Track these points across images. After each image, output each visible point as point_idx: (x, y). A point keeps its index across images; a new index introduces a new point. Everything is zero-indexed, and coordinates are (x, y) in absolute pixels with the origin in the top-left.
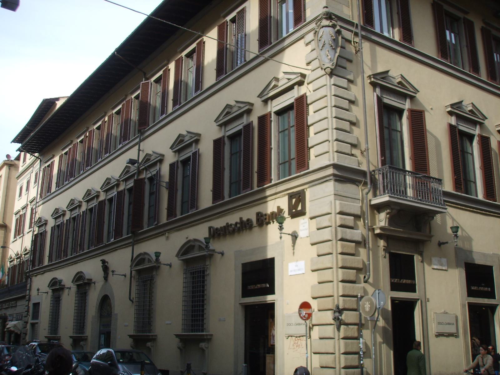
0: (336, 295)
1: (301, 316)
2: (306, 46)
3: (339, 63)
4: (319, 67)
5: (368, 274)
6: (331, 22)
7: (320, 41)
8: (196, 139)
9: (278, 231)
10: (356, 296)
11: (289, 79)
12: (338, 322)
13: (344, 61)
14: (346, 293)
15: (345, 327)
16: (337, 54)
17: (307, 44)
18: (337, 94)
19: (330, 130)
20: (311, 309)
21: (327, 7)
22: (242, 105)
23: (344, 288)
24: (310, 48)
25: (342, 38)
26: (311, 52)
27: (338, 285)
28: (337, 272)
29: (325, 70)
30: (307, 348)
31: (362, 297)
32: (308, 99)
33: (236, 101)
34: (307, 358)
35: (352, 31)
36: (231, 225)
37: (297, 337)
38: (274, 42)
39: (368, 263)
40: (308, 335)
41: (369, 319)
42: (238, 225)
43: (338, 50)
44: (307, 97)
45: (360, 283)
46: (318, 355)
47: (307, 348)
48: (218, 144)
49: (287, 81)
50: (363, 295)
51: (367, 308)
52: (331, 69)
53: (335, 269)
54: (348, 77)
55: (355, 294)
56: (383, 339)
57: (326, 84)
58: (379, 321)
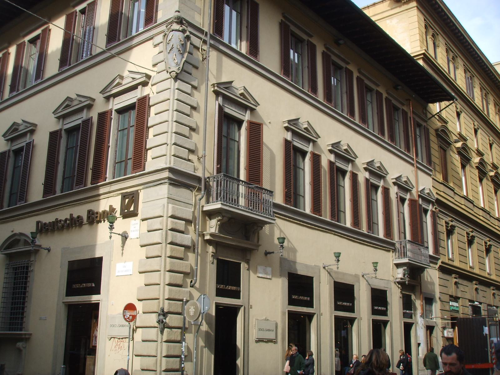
0: (161, 298)
1: (126, 317)
2: (154, 47)
3: (185, 68)
4: (165, 70)
5: (195, 279)
6: (181, 26)
7: (168, 44)
8: (32, 129)
9: (109, 230)
10: (181, 300)
11: (133, 78)
12: (162, 325)
13: (191, 67)
14: (172, 297)
15: (169, 330)
16: (184, 60)
17: (155, 46)
18: (180, 98)
19: (169, 134)
20: (136, 311)
21: (179, 12)
22: (83, 100)
23: (170, 291)
24: (158, 49)
25: (191, 44)
26: (158, 54)
27: (164, 287)
28: (164, 274)
29: (170, 73)
30: (129, 350)
31: (187, 301)
32: (151, 100)
33: (77, 95)
34: (128, 360)
35: (201, 39)
36: (60, 221)
37: (119, 339)
38: (122, 40)
39: (196, 267)
40: (131, 337)
41: (192, 323)
42: (68, 222)
43: (186, 55)
44: (149, 98)
45: (186, 287)
46: (140, 357)
47: (129, 350)
48: (54, 136)
49: (131, 80)
50: (189, 299)
51: (192, 313)
52: (176, 73)
53: (162, 272)
54: (193, 83)
55: (181, 298)
56: (205, 344)
57: (170, 87)
58: (202, 325)
